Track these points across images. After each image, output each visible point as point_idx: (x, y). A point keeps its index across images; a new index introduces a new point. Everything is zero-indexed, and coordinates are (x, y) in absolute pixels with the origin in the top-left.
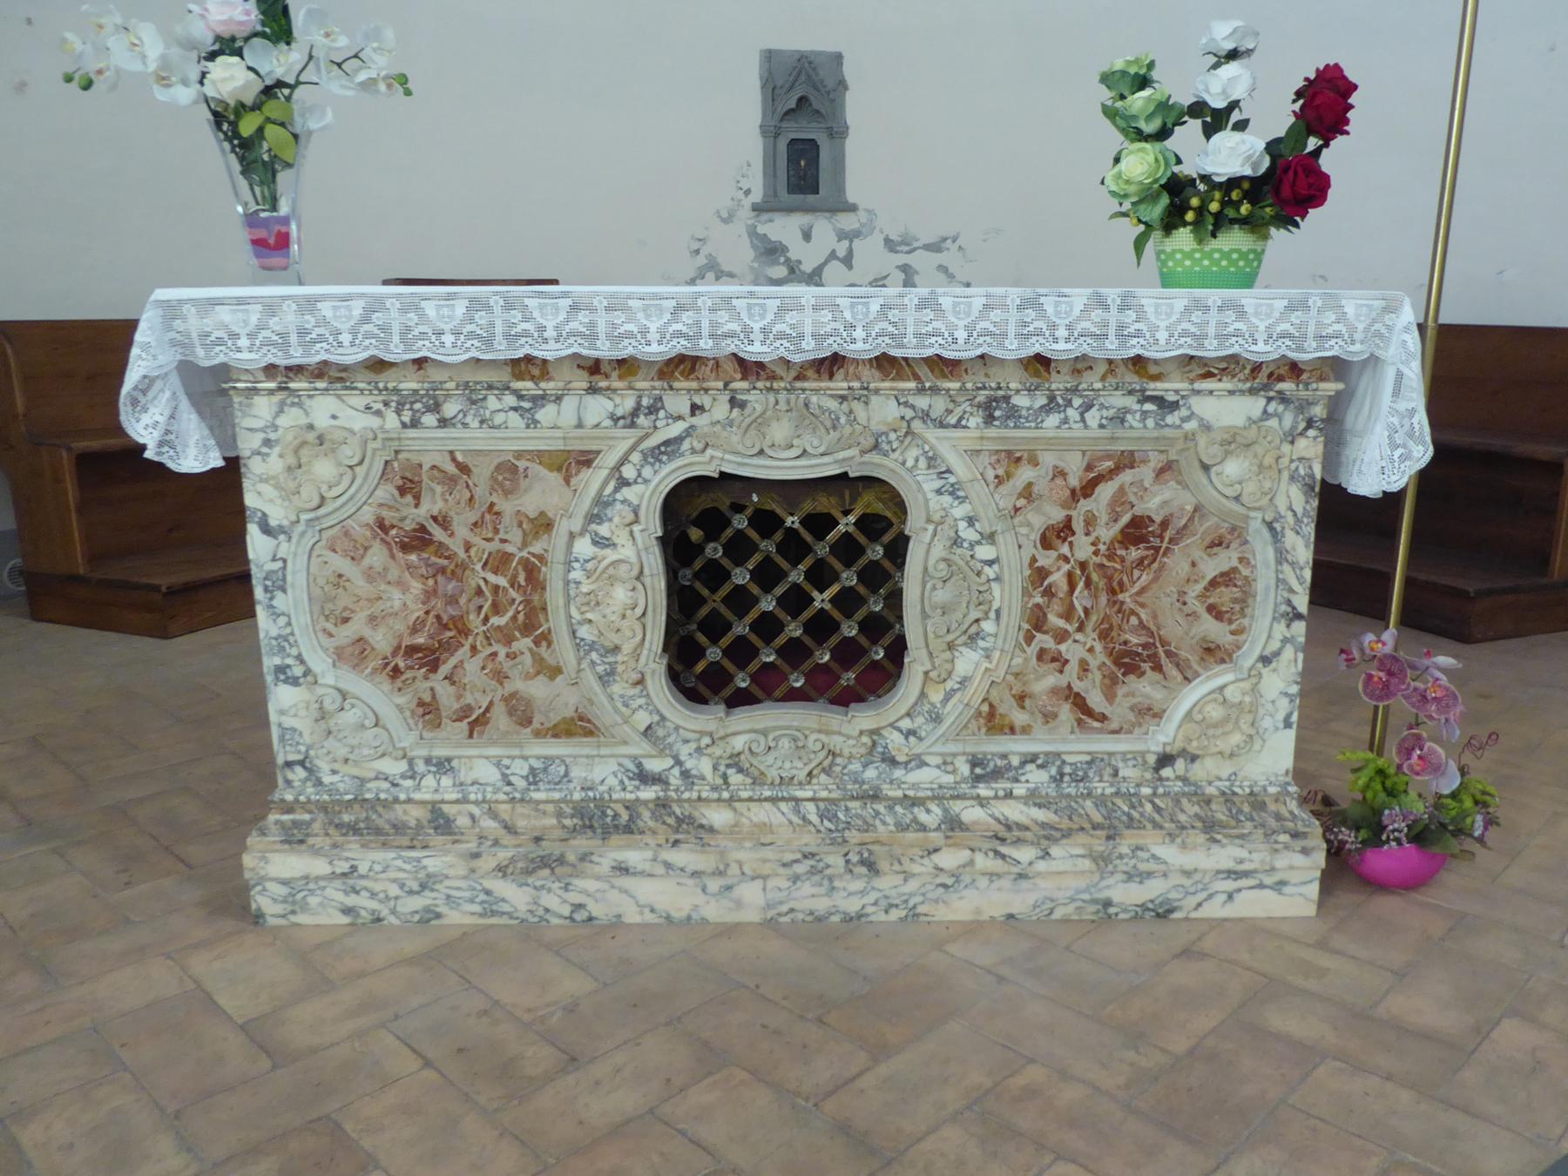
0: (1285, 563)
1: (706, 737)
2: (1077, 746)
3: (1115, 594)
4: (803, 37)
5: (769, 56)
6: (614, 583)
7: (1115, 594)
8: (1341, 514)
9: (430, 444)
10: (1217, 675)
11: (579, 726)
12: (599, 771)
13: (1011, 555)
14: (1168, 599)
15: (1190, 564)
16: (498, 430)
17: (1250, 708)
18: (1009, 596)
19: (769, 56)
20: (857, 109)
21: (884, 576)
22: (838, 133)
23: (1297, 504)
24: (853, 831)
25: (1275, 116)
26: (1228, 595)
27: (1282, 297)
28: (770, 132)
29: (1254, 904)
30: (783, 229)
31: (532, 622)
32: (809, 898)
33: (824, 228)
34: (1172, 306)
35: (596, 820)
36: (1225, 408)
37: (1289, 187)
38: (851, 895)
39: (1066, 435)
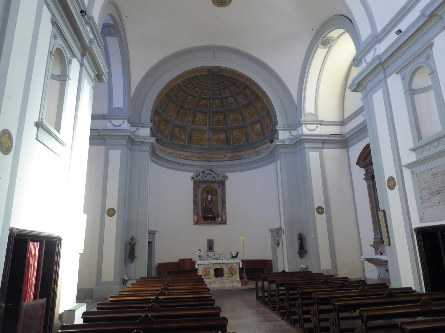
0: (238, 271)
1: (216, 279)
2: (231, 279)
3: (232, 272)
4: (210, 238)
5: (208, 240)
6: (212, 272)
7: (232, 272)
8: (240, 268)
9: (206, 267)
10: (102, 56)
11: (211, 278)
12: (212, 281)
13: (227, 271)
14: (234, 272)
15: (234, 271)
16: (208, 266)
17: (237, 277)
18: (228, 272)
19: (208, 240)
20: (215, 243)
21: (220, 277)
22: (213, 245)
23: (238, 268)
24: (222, 283)
25: (236, 254)
26: (236, 272)
27: (238, 260)
28: (208, 246)
29: (238, 285)
30: (209, 253)
31: (209, 274)
32: (220, 286)
33: (212, 253)
34: (232, 261)
35: (212, 282)
36: (235, 265)
37: (236, 256)
38: (222, 285)
39: (229, 266)
